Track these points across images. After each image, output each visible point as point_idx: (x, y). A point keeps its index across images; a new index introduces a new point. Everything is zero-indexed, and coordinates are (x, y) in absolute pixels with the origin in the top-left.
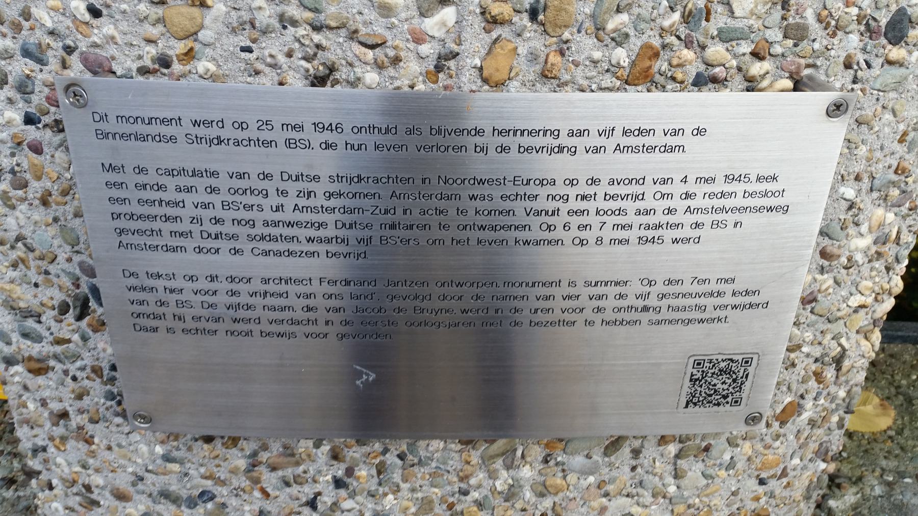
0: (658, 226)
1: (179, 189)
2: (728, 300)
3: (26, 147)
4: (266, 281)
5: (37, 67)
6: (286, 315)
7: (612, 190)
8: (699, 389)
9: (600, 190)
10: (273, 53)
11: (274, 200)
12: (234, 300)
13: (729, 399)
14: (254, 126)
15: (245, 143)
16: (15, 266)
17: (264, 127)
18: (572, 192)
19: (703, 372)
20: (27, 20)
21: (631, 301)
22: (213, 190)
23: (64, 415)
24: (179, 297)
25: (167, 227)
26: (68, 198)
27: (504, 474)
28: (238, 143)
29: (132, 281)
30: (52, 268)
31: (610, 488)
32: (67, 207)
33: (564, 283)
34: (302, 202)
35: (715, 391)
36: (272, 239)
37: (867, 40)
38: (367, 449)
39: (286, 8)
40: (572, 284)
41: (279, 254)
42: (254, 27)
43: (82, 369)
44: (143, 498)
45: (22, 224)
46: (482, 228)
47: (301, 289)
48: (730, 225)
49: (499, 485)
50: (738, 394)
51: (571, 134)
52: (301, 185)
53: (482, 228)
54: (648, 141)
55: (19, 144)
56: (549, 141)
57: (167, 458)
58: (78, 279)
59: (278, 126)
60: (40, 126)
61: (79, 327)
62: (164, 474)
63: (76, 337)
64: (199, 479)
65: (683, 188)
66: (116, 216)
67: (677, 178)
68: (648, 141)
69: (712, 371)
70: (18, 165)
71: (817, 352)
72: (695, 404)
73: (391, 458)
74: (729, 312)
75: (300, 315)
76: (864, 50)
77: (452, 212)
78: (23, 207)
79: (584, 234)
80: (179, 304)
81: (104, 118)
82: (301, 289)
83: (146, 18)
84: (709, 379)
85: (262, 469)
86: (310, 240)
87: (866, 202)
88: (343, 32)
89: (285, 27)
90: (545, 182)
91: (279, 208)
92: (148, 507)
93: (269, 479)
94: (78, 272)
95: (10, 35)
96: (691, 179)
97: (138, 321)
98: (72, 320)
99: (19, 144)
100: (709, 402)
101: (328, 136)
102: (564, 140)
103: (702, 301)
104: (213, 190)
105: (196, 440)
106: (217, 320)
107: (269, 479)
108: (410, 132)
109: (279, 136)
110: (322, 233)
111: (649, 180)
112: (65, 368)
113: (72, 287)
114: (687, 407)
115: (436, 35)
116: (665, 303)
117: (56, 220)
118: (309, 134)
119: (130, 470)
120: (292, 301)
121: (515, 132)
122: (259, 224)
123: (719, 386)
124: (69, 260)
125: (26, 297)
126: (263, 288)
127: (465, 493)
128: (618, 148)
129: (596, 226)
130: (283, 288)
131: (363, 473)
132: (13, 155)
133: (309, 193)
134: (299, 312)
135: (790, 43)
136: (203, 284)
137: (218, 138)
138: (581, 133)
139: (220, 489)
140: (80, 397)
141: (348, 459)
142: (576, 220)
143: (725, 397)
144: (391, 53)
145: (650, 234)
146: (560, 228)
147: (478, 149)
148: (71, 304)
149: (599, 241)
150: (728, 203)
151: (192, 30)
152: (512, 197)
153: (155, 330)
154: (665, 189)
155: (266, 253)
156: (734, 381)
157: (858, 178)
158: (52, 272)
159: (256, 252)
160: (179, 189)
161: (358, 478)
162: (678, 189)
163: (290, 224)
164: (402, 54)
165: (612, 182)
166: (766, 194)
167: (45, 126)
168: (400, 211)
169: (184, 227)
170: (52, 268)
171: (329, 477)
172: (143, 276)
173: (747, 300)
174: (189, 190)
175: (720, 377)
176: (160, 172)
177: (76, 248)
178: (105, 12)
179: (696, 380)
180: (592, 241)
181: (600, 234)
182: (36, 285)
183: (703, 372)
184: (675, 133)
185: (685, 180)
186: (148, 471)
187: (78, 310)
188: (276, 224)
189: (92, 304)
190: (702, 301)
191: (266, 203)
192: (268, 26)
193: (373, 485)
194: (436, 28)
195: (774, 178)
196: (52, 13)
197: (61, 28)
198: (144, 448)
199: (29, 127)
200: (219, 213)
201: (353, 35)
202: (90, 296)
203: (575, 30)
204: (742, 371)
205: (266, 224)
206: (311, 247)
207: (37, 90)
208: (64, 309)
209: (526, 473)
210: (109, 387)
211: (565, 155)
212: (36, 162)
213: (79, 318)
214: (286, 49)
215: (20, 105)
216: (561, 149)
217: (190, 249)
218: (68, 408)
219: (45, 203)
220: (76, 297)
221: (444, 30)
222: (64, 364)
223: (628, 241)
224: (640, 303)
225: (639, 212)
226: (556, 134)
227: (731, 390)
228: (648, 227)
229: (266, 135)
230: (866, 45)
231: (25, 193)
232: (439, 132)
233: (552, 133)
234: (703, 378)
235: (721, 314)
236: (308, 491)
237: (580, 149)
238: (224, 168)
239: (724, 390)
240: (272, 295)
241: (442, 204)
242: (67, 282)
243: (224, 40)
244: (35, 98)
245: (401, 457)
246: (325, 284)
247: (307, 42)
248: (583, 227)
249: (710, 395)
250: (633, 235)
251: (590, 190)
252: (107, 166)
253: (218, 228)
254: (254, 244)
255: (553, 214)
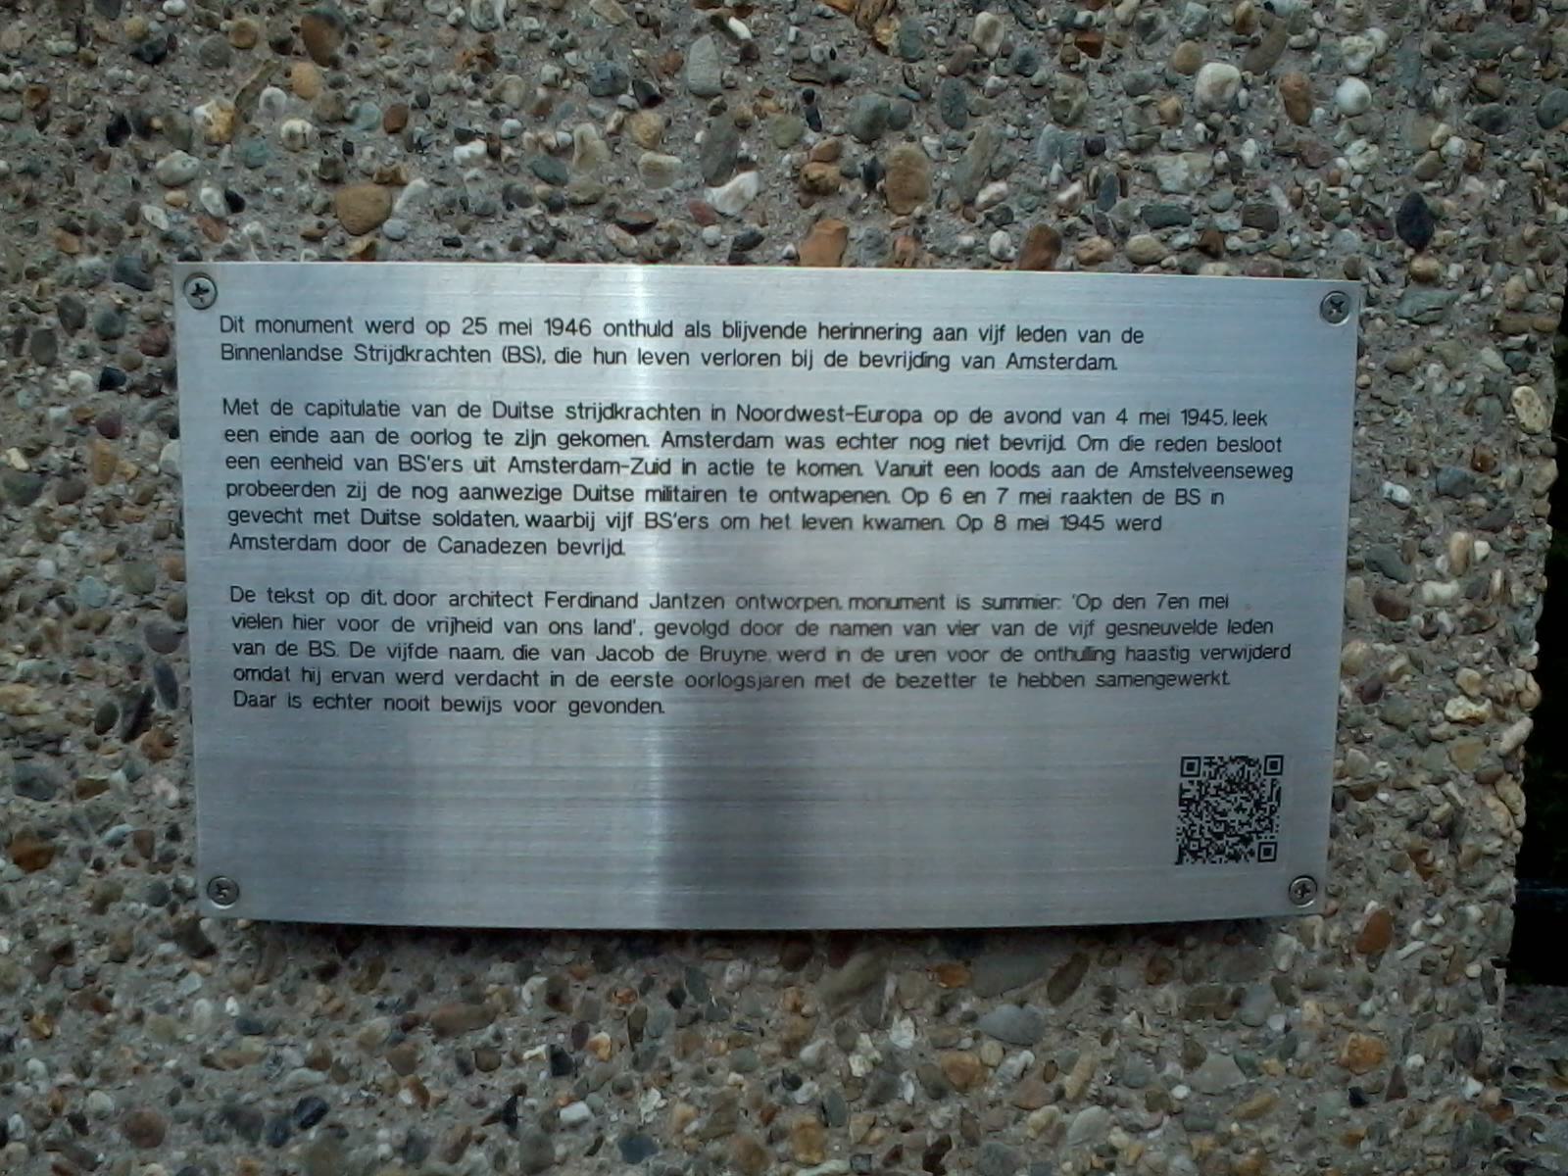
0: (1091, 498)
1: (336, 438)
2: (1222, 639)
3: (93, 429)
4: (456, 601)
5: (134, 294)
6: (485, 666)
7: (1014, 431)
8: (1197, 821)
9: (995, 430)
10: (491, 244)
11: (480, 451)
12: (405, 638)
13: (1254, 845)
14: (457, 326)
15: (443, 355)
16: (34, 648)
17: (472, 329)
18: (950, 434)
19: (1200, 783)
20: (131, 223)
21: (1063, 639)
22: (387, 437)
23: (63, 952)
24: (315, 636)
25: (310, 505)
26: (150, 507)
27: (865, 1040)
28: (431, 357)
29: (244, 609)
30: (99, 645)
31: (1070, 1082)
32: (144, 525)
33: (950, 602)
34: (524, 454)
35: (1227, 827)
36: (474, 521)
37: (1373, 239)
38: (612, 980)
39: (515, 179)
40: (963, 604)
41: (482, 549)
42: (466, 209)
43: (116, 843)
44: (184, 1130)
45: (63, 564)
46: (809, 497)
47: (513, 615)
48: (1206, 499)
49: (858, 1067)
50: (1268, 833)
51: (939, 335)
52: (522, 425)
53: (809, 497)
54: (1059, 349)
55: (84, 423)
56: (904, 346)
57: (248, 1027)
58: (141, 657)
59: (493, 327)
60: (123, 388)
61: (127, 756)
62: (237, 1065)
63: (118, 776)
64: (305, 1071)
65: (1121, 432)
66: (233, 490)
67: (1111, 414)
68: (1059, 349)
69: (1213, 783)
70: (75, 459)
71: (1406, 804)
72: (1194, 854)
73: (657, 1006)
74: (1227, 664)
75: (509, 666)
76: (1370, 254)
77: (761, 468)
78: (70, 535)
79: (973, 510)
80: (316, 649)
81: (237, 324)
82: (513, 615)
83: (309, 204)
84: (1212, 800)
85: (422, 1036)
86: (533, 521)
87: (1435, 514)
88: (594, 211)
89: (510, 207)
90: (905, 416)
91: (485, 466)
92: (192, 1154)
93: (434, 1056)
94: (142, 643)
95: (103, 249)
96: (1132, 416)
97: (241, 685)
98: (116, 742)
99: (84, 423)
100: (1220, 852)
101: (567, 341)
102: (929, 346)
103: (1181, 641)
104: (387, 437)
105: (305, 976)
106: (370, 678)
107: (434, 1056)
108: (692, 331)
109: (494, 342)
110: (553, 509)
111: (1067, 416)
112: (84, 844)
113: (127, 677)
114: (1179, 862)
115: (729, 211)
116: (1120, 643)
117: (122, 550)
118: (539, 338)
119: (171, 1063)
120: (498, 638)
121: (853, 331)
122: (454, 495)
123: (1232, 816)
124: (132, 622)
125: (42, 705)
126: (451, 612)
127: (794, 1083)
128: (1012, 361)
129: (993, 495)
130: (482, 613)
131: (604, 1037)
132: (71, 443)
133: (535, 437)
134: (509, 659)
135: (1254, 233)
136: (355, 610)
137: (403, 349)
138: (953, 335)
139: (335, 1089)
140: (101, 906)
141: (576, 1003)
142: (959, 486)
143: (1246, 840)
144: (665, 238)
145: (1081, 511)
146: (935, 497)
147: (798, 360)
148: (120, 710)
149: (1000, 522)
150: (1199, 459)
151: (375, 219)
152: (855, 443)
153: (268, 702)
154: (1094, 431)
155: (460, 548)
156: (1258, 805)
157: (1412, 471)
158: (99, 651)
159: (445, 545)
160: (336, 438)
161: (595, 1048)
162: (1113, 432)
163: (502, 494)
164: (682, 240)
165: (1009, 419)
166: (1253, 445)
167: (133, 388)
168: (676, 468)
169: (337, 503)
170: (99, 645)
171: (541, 1049)
172: (261, 599)
173: (1254, 640)
174: (350, 438)
175: (1232, 797)
176: (311, 409)
177: (147, 598)
178: (248, 202)
179: (1191, 801)
180: (989, 521)
181: (1000, 509)
182: (66, 680)
183: (1200, 783)
184: (1096, 337)
185: (1122, 418)
186: (207, 1062)
187: (131, 718)
188: (480, 494)
189: (158, 706)
190: (1181, 641)
191: (467, 457)
192: (486, 205)
193: (623, 1070)
194: (729, 201)
195: (1261, 419)
196: (171, 209)
197: (182, 232)
198: (204, 1006)
199: (105, 394)
200: (392, 476)
201: (610, 215)
202: (156, 690)
203: (932, 204)
204: (1268, 784)
205: (465, 494)
206: (533, 535)
207: (129, 328)
208: (104, 723)
209: (903, 1034)
210: (160, 876)
211: (933, 370)
212: (107, 449)
213: (130, 736)
214: (509, 239)
215: (98, 359)
216: (925, 360)
217: (342, 543)
218: (75, 936)
219: (107, 522)
220: (132, 695)
221: (741, 206)
222: (86, 838)
223: (1046, 523)
224: (1078, 643)
225: (1057, 472)
226: (915, 335)
227: (1254, 825)
228: (1075, 500)
229: (474, 342)
230: (1373, 247)
231: (79, 507)
232: (736, 332)
233: (910, 333)
234: (1202, 797)
235: (1217, 666)
236: (501, 1083)
237: (956, 361)
238: (406, 398)
239: (1241, 824)
240: (466, 627)
241: (744, 455)
242: (118, 668)
243: (421, 232)
244: (123, 345)
245: (675, 999)
246: (553, 604)
247: (541, 227)
248: (971, 497)
249: (1219, 836)
250: (1054, 512)
251: (978, 431)
252: (231, 403)
253: (390, 504)
254: (444, 530)
255: (922, 473)
